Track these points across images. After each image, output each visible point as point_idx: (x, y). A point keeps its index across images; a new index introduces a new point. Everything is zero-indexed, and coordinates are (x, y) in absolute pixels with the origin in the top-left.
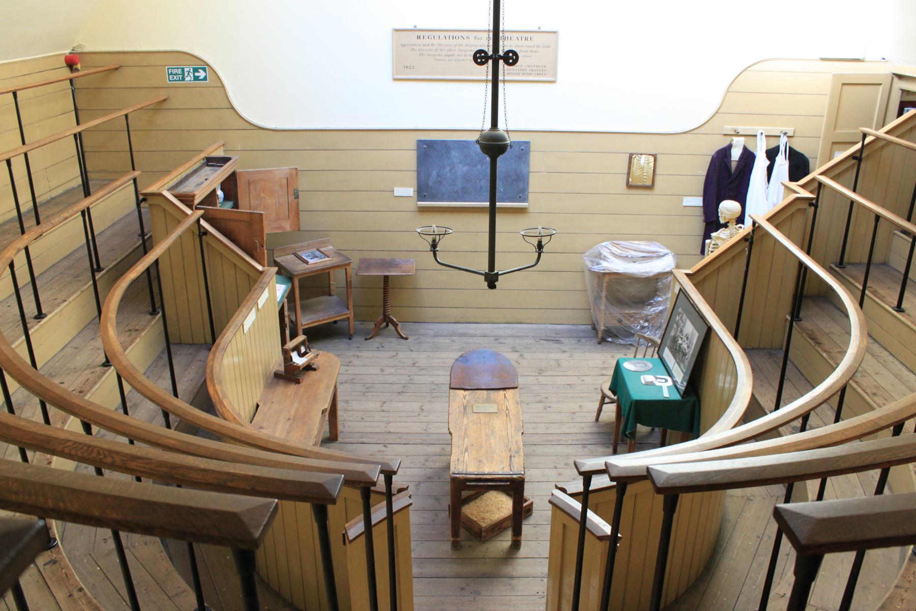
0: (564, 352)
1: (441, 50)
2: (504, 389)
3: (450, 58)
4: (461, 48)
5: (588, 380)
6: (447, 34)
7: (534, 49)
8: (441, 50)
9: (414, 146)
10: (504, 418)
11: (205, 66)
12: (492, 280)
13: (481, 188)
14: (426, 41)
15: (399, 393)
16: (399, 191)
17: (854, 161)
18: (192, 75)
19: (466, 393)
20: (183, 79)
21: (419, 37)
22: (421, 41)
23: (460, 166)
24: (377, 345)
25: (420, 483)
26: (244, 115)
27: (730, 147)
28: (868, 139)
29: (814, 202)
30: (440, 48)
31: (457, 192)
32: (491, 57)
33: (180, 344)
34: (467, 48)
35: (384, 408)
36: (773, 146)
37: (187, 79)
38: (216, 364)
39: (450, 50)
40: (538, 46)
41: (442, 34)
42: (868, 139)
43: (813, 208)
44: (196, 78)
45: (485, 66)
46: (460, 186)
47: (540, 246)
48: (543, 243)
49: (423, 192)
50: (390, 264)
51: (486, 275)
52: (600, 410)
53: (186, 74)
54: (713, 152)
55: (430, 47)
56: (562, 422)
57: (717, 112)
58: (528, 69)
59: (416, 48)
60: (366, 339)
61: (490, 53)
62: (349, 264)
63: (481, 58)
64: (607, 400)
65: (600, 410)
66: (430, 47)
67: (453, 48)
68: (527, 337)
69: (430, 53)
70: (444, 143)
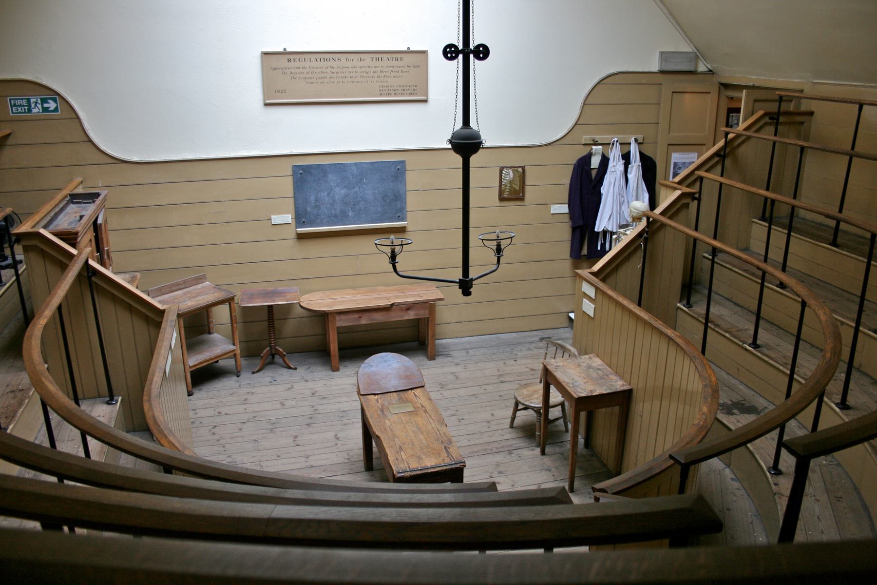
3: (323, 80)
4: (333, 70)
5: (490, 388)
7: (404, 70)
9: (290, 172)
10: (424, 415)
11: (56, 95)
12: (466, 286)
13: (360, 210)
15: (308, 425)
16: (276, 219)
17: (717, 159)
18: (40, 106)
19: (376, 397)
20: (30, 111)
21: (289, 60)
22: (292, 64)
23: (337, 189)
24: (268, 379)
26: (103, 147)
27: (588, 158)
28: (730, 136)
29: (697, 196)
31: (336, 216)
32: (462, 52)
33: (84, 399)
34: (338, 70)
35: (298, 442)
36: (625, 151)
37: (35, 110)
40: (409, 66)
41: (313, 57)
42: (730, 136)
43: (696, 202)
44: (46, 110)
45: (456, 61)
46: (338, 211)
47: (499, 250)
48: (502, 247)
49: (300, 218)
52: (513, 418)
53: (33, 105)
54: (575, 162)
56: (480, 432)
58: (400, 89)
59: (286, 71)
61: (461, 47)
62: (232, 299)
63: (451, 52)
64: (520, 407)
65: (513, 418)
68: (799, 296)
69: (302, 76)
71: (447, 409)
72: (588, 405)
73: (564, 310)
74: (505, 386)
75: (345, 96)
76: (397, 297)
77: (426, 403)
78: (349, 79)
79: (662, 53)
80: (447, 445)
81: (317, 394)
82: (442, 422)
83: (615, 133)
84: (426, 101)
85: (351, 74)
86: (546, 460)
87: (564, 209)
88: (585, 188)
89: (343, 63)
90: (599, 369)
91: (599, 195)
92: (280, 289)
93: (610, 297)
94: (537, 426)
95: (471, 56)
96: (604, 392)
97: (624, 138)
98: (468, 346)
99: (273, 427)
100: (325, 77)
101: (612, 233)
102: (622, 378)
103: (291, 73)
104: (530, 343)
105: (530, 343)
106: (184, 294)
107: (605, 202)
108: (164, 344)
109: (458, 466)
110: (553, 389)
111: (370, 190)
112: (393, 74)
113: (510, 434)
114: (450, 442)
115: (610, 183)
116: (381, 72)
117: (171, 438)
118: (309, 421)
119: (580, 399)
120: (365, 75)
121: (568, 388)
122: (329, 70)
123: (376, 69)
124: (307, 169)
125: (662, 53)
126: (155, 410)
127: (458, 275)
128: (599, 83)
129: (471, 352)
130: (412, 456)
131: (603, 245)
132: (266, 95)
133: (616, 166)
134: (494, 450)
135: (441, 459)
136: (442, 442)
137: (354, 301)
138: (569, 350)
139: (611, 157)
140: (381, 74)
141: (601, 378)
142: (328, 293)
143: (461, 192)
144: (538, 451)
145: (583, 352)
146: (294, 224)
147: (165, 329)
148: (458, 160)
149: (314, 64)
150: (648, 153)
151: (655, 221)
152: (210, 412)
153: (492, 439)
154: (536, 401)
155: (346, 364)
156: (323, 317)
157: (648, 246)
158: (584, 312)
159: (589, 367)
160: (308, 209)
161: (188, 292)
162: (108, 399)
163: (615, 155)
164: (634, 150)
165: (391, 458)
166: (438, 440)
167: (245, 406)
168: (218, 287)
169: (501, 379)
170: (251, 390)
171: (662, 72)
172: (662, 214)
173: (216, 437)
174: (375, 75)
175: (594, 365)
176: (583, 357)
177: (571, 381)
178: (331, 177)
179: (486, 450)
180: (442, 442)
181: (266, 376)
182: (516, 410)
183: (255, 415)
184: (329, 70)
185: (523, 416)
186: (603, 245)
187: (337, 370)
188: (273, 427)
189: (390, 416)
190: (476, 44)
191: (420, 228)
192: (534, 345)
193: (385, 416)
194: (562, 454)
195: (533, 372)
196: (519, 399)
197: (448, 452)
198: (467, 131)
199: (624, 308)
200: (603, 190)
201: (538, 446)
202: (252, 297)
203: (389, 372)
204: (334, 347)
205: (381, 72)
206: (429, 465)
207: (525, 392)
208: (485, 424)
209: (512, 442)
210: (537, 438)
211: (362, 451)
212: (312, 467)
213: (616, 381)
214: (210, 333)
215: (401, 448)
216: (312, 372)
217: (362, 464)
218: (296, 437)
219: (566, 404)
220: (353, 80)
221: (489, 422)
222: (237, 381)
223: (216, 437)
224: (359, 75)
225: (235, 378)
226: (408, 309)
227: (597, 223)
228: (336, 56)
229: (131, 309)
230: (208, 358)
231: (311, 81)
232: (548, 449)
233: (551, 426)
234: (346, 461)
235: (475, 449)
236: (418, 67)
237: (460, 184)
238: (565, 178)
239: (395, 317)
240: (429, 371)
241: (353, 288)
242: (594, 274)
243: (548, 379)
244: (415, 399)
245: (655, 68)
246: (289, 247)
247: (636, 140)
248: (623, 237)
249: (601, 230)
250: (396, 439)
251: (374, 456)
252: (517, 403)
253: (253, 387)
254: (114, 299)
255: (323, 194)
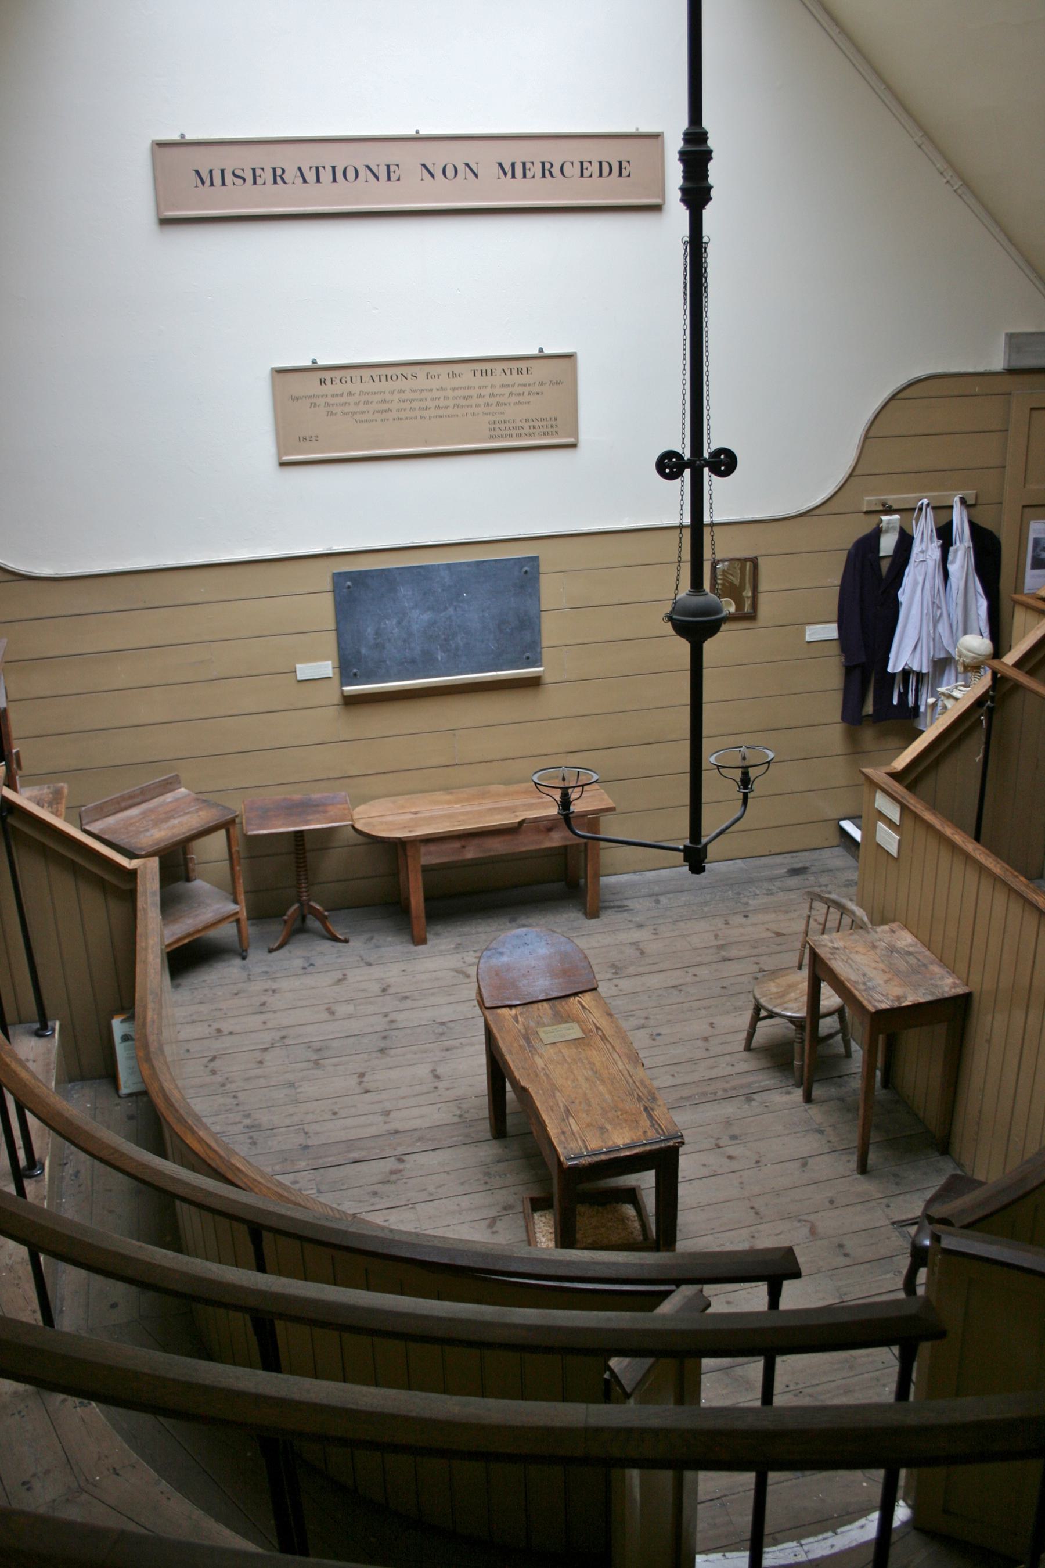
0: (640, 926)
1: (367, 402)
2: (576, 994)
3: (384, 416)
4: (404, 396)
5: (703, 972)
6: (375, 372)
7: (534, 389)
8: (367, 402)
10: (601, 1045)
12: (695, 859)
13: (457, 649)
14: (338, 388)
15: (382, 1051)
16: (305, 671)
19: (513, 1011)
21: (323, 382)
22: (328, 389)
23: (415, 614)
25: (493, 1221)
27: (876, 535)
30: (364, 398)
31: (413, 661)
32: (689, 464)
34: (412, 396)
36: (943, 522)
38: (166, 1085)
39: (384, 401)
40: (542, 384)
41: (366, 373)
45: (679, 480)
47: (746, 782)
49: (349, 667)
50: (305, 807)
51: (686, 850)
54: (850, 546)
55: (345, 399)
57: (851, 475)
58: (526, 425)
60: (271, 951)
61: (687, 455)
62: (232, 821)
64: (763, 1013)
66: (345, 399)
67: (388, 397)
69: (347, 409)
70: (383, 574)
71: (629, 1015)
72: (891, 1025)
73: (833, 814)
74: (732, 969)
75: (426, 443)
76: (531, 807)
77: (603, 1022)
78: (433, 412)
79: (1010, 336)
80: (649, 1104)
81: (391, 991)
82: (635, 1059)
83: (924, 488)
84: (574, 446)
85: (437, 403)
86: (815, 1112)
87: (830, 631)
88: (869, 594)
89: (422, 382)
90: (909, 953)
91: (896, 605)
92: (315, 796)
93: (929, 827)
94: (797, 1047)
95: (706, 470)
96: (922, 1000)
97: (939, 496)
98: (656, 889)
99: (319, 1055)
100: (389, 410)
101: (920, 676)
102: (953, 971)
103: (327, 404)
104: (771, 879)
105: (771, 879)
106: (144, 814)
107: (905, 626)
108: (151, 942)
109: (671, 1143)
110: (826, 989)
111: (475, 613)
112: (514, 399)
113: (746, 1063)
114: (654, 1099)
115: (915, 583)
116: (492, 395)
117: (201, 1133)
118: (382, 1044)
119: (880, 1013)
120: (462, 402)
121: (856, 993)
122: (396, 396)
123: (483, 392)
124: (359, 579)
125: (1010, 336)
126: (162, 1077)
127: (680, 833)
128: (893, 398)
129: (663, 900)
130: (589, 1125)
131: (903, 697)
132: (282, 445)
133: (926, 549)
134: (720, 1094)
135: (640, 1133)
136: (639, 1099)
137: (450, 817)
138: (853, 913)
139: (917, 536)
140: (491, 400)
141: (915, 971)
142: (401, 800)
143: (705, 732)
144: (798, 1094)
145: (880, 918)
146: (337, 680)
147: (145, 910)
148: (683, 647)
149: (369, 386)
150: (986, 523)
151: (1005, 679)
152: (201, 1030)
153: (714, 1073)
154: (794, 1005)
155: (439, 928)
156: (394, 851)
157: (996, 722)
158: (879, 846)
159: (892, 949)
160: (364, 651)
161: (151, 811)
162: (37, 1026)
163: (924, 529)
164: (959, 518)
165: (553, 1131)
166: (631, 1094)
167: (263, 1017)
168: (202, 799)
169: (723, 953)
170: (270, 985)
171: (1011, 372)
172: (1018, 665)
173: (218, 1079)
174: (481, 401)
175: (900, 944)
176: (880, 929)
177: (861, 979)
178: (402, 591)
179: (705, 1094)
180: (639, 1099)
181: (294, 956)
182: (756, 1018)
183: (283, 1033)
184: (396, 396)
185: (765, 1028)
186: (903, 697)
187: (423, 941)
188: (319, 1055)
189: (542, 1051)
190: (713, 448)
191: (565, 678)
192: (778, 884)
193: (534, 1050)
194: (842, 1099)
195: (780, 939)
196: (763, 1001)
197: (650, 1117)
198: (699, 600)
199: (954, 847)
200: (903, 596)
201: (798, 1085)
202: (265, 814)
203: (533, 963)
204: (417, 901)
205: (492, 395)
206: (620, 1142)
207: (773, 987)
208: (700, 1043)
209: (751, 1078)
210: (797, 1073)
211: (485, 1100)
212: (397, 1132)
213: (942, 978)
214: (188, 879)
215: (568, 1112)
216: (377, 947)
217: (486, 1126)
218: (362, 1075)
219: (847, 1010)
220: (440, 412)
221: (706, 1039)
222: (244, 968)
223: (218, 1079)
224: (451, 403)
225: (237, 962)
226: (550, 829)
227: (892, 655)
228: (408, 371)
229: (75, 869)
230: (192, 930)
231: (363, 417)
232: (817, 1092)
233: (821, 1049)
234: (456, 1120)
235: (686, 1092)
236: (558, 383)
237: (686, 699)
238: (831, 576)
239: (527, 843)
240: (593, 939)
241: (447, 789)
242: (895, 776)
243: (819, 971)
244: (583, 1015)
245: (998, 362)
246: (329, 719)
247: (963, 501)
248: (949, 703)
249: (899, 669)
250: (558, 1094)
251: (509, 1110)
252: (758, 1008)
253: (274, 979)
254: (45, 853)
255: (391, 623)
